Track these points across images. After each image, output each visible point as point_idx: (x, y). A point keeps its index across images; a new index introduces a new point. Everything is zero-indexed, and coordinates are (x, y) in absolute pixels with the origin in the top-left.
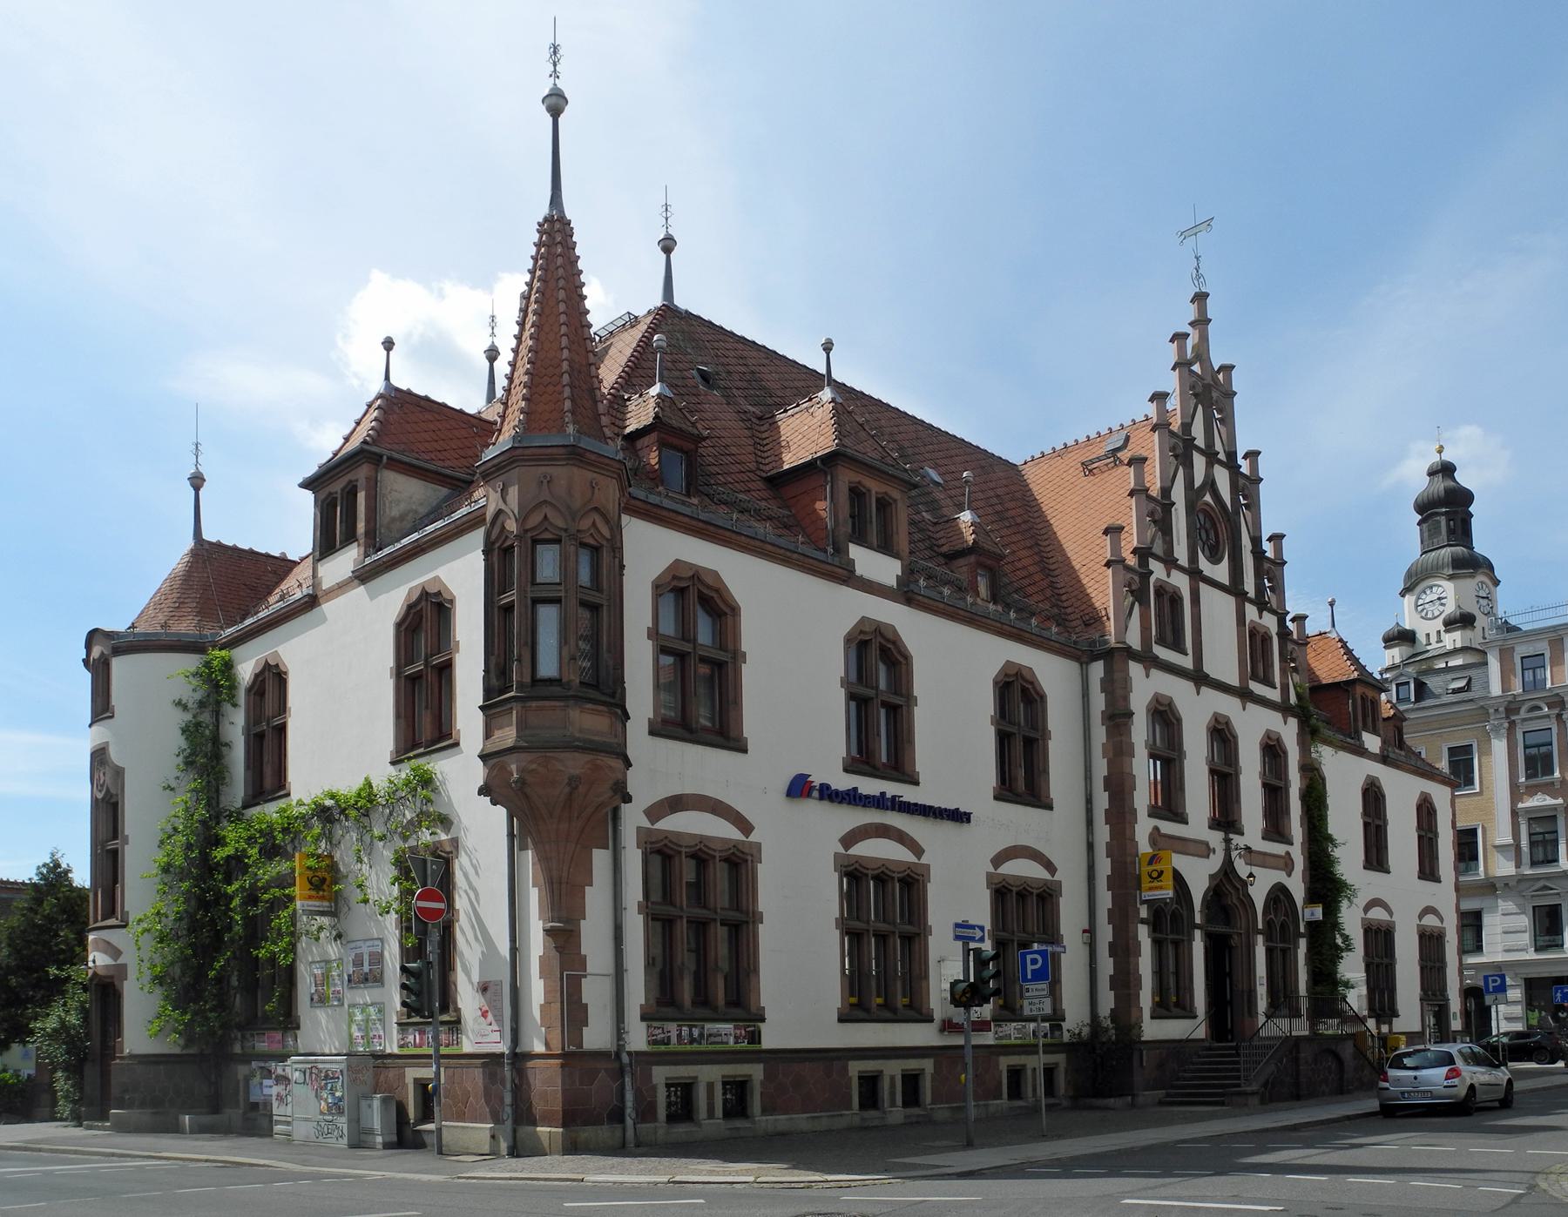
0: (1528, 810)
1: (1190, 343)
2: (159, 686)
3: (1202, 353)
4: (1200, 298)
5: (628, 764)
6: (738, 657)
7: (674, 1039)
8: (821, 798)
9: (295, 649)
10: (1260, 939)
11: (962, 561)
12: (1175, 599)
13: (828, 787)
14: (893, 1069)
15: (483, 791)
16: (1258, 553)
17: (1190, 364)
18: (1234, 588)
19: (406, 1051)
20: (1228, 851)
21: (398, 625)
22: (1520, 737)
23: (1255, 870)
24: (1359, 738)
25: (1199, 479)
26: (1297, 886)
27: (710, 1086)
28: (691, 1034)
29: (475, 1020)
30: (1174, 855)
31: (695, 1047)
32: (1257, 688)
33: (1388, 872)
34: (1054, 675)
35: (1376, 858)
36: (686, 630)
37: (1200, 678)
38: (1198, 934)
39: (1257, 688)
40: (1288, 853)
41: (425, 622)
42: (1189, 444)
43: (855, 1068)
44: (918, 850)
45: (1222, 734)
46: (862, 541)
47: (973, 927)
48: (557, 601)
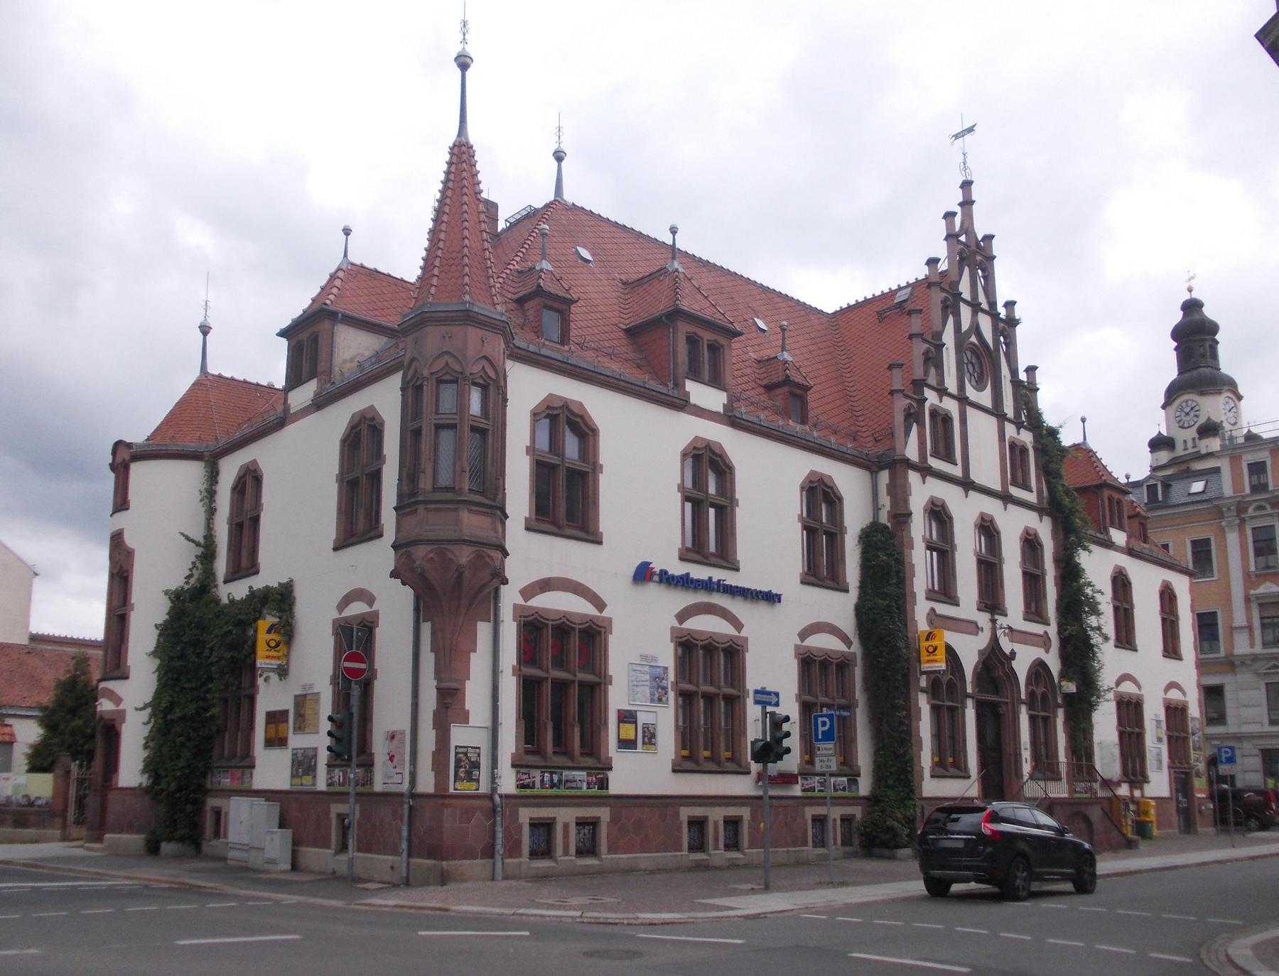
0: (1258, 597)
1: (958, 220)
2: (169, 492)
3: (967, 228)
4: (966, 185)
5: (506, 554)
6: (596, 468)
7: (538, 784)
8: (661, 581)
9: (268, 454)
10: (1023, 709)
11: (778, 391)
12: (947, 419)
13: (666, 572)
14: (716, 815)
15: (394, 574)
16: (1016, 383)
17: (958, 236)
18: (996, 411)
19: (332, 789)
20: (994, 630)
21: (344, 441)
22: (1249, 532)
23: (1019, 648)
24: (1107, 533)
25: (965, 325)
26: (1053, 661)
27: (566, 826)
28: (552, 780)
29: (384, 763)
30: (946, 632)
31: (554, 791)
32: (1015, 492)
33: (1136, 650)
34: (849, 482)
35: (1125, 638)
36: (555, 443)
37: (967, 484)
38: (970, 704)
39: (1015, 492)
40: (1046, 633)
41: (362, 436)
42: (958, 296)
43: (686, 813)
44: (738, 625)
45: (987, 529)
46: (697, 378)
47: (769, 693)
48: (453, 427)
